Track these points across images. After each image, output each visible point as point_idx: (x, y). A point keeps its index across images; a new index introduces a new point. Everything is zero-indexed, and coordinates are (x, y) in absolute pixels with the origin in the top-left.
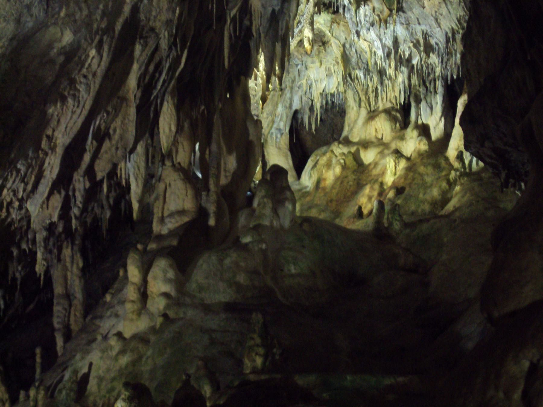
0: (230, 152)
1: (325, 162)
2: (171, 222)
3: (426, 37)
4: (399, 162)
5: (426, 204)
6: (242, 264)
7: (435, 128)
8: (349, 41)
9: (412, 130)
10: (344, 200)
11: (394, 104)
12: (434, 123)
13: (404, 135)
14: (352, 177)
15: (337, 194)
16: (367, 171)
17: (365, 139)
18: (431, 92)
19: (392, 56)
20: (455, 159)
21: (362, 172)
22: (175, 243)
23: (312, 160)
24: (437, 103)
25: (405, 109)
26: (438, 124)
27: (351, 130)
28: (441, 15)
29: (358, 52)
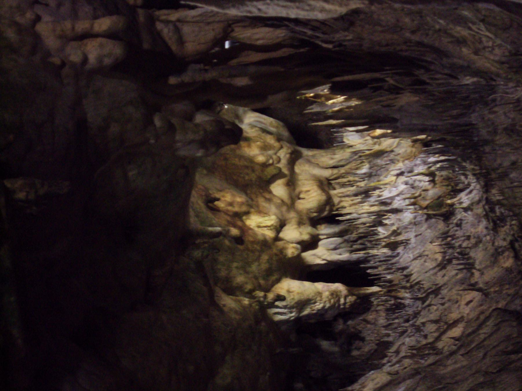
1: (268, 143)
2: (169, 32)
3: (403, 243)
4: (271, 230)
5: (227, 272)
7: (314, 255)
8: (397, 157)
9: (309, 234)
11: (337, 206)
12: (320, 254)
14: (253, 177)
15: (234, 164)
16: (261, 191)
17: (298, 180)
18: (351, 247)
20: (276, 294)
22: (146, 46)
23: (272, 122)
24: (340, 254)
27: (309, 161)
28: (425, 261)
29: (387, 166)
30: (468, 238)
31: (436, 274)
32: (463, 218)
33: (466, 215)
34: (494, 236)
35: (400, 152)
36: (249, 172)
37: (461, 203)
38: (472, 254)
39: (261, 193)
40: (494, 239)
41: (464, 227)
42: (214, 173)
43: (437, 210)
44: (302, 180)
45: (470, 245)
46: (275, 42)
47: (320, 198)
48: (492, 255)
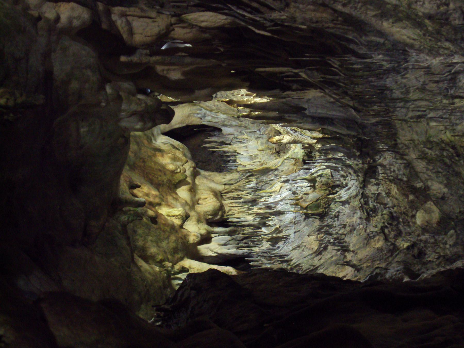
0: (184, 73)
1: (177, 156)
2: (122, 23)
4: (178, 218)
5: (143, 242)
6: (87, 86)
10: (145, 173)
11: (227, 213)
14: (165, 179)
15: (150, 167)
16: (170, 191)
18: (238, 244)
19: (268, 211)
21: (169, 188)
23: (179, 144)
25: (224, 223)
27: (206, 177)
28: (303, 251)
29: (271, 182)
30: (345, 226)
32: (341, 211)
33: (343, 208)
34: (367, 224)
35: (283, 169)
37: (341, 197)
38: (347, 239)
39: (170, 193)
40: (366, 227)
41: (341, 218)
42: (134, 170)
43: (316, 210)
44: (200, 190)
45: (345, 233)
46: (216, 25)
47: (216, 204)
48: (365, 239)
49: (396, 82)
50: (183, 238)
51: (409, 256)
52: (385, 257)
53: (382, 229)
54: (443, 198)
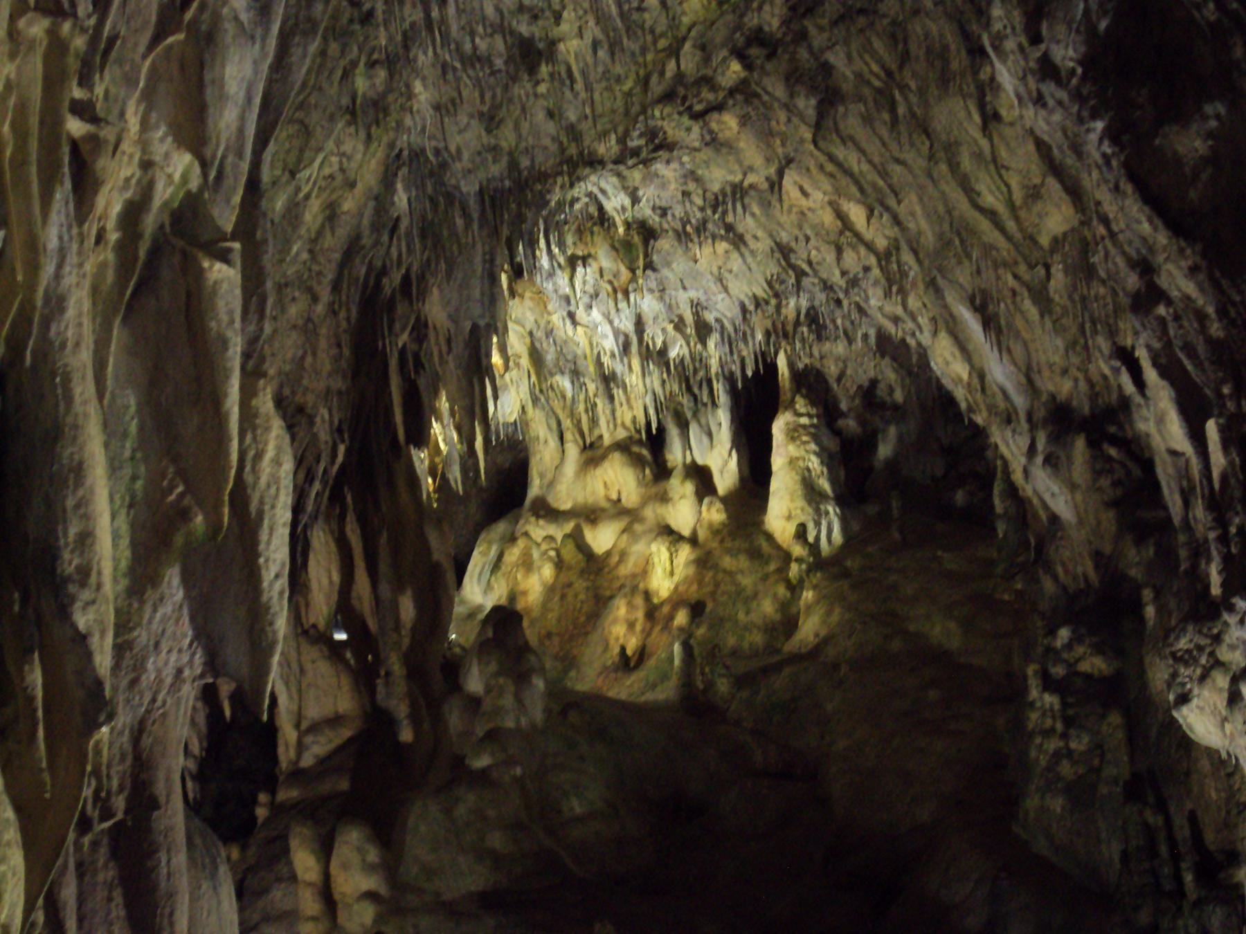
4: (677, 551)
5: (755, 631)
6: (491, 813)
7: (722, 473)
10: (576, 632)
12: (720, 462)
13: (665, 492)
14: (580, 585)
15: (559, 620)
16: (606, 570)
19: (634, 348)
21: (599, 571)
22: (344, 785)
25: (656, 441)
26: (726, 463)
27: (551, 484)
28: (731, 271)
30: (686, 194)
31: (752, 252)
33: (644, 200)
36: (570, 593)
37: (624, 209)
38: (716, 187)
45: (700, 192)
48: (718, 150)
49: (470, 171)
50: (719, 537)
51: (769, 66)
52: (762, 110)
53: (696, 116)
54: (703, 48)
